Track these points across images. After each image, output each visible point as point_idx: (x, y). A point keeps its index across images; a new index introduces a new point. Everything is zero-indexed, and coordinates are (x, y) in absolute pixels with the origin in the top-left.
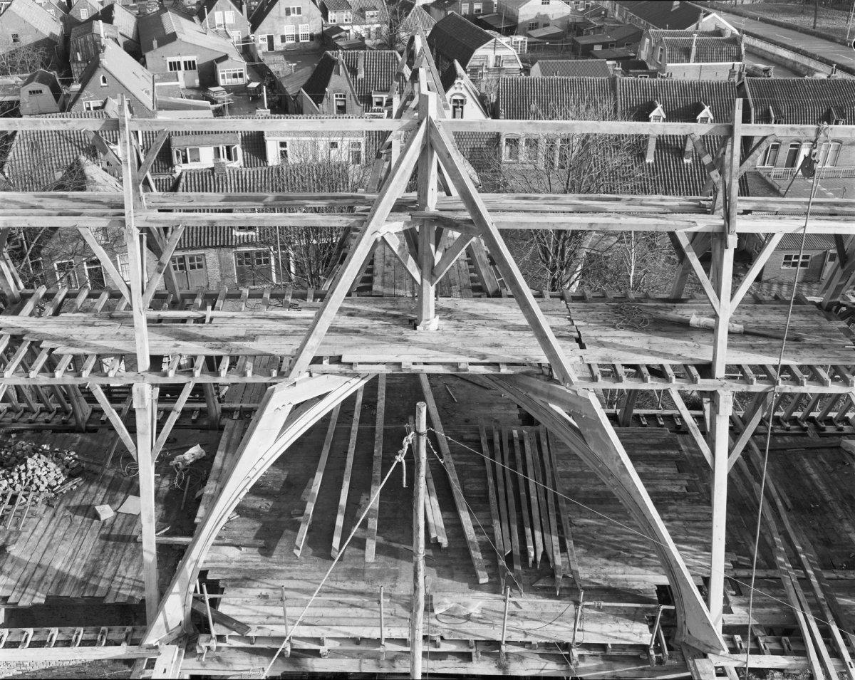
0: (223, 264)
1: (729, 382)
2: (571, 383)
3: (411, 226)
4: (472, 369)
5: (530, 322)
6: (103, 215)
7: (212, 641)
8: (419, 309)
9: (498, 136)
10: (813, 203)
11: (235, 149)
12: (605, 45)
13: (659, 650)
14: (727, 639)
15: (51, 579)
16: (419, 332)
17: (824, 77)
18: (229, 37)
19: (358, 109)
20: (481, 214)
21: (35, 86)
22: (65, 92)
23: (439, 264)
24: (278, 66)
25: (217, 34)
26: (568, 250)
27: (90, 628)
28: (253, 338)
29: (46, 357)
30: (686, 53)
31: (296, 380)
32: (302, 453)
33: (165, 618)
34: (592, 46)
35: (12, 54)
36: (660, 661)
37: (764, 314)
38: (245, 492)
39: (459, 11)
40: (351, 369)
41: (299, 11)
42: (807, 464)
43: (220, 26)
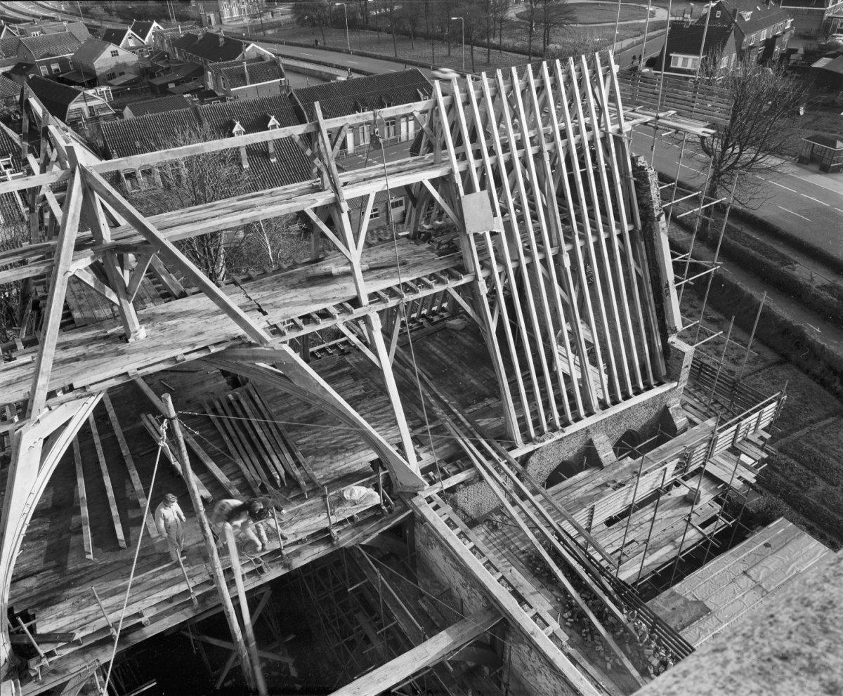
1: (373, 306)
2: (267, 342)
3: (96, 260)
4: (188, 358)
7: (43, 661)
9: (118, 173)
10: (388, 167)
12: (177, 83)
13: (387, 504)
14: (425, 478)
16: (132, 343)
17: (343, 79)
26: (212, 250)
30: (241, 79)
31: (38, 417)
32: (63, 475)
34: (166, 85)
36: (390, 511)
37: (377, 252)
38: (26, 527)
39: (39, 72)
40: (86, 391)
42: (431, 346)
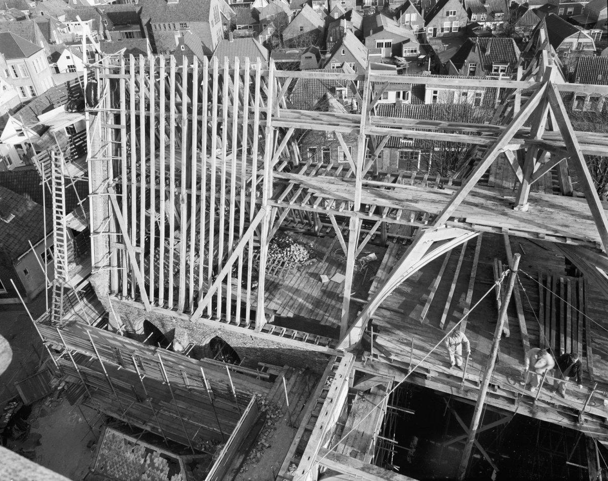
0: (392, 157)
4: (547, 238)
5: (593, 215)
6: (349, 126)
8: (518, 196)
11: (408, 94)
15: (296, 306)
18: (412, 29)
19: (483, 73)
20: (573, 144)
21: (309, 54)
22: (322, 57)
23: (536, 172)
24: (437, 46)
25: (404, 28)
27: (312, 335)
28: (416, 201)
29: (310, 196)
31: (438, 228)
32: (432, 268)
33: (350, 338)
35: (299, 37)
39: (557, 13)
40: (471, 226)
41: (454, 13)
43: (407, 22)
